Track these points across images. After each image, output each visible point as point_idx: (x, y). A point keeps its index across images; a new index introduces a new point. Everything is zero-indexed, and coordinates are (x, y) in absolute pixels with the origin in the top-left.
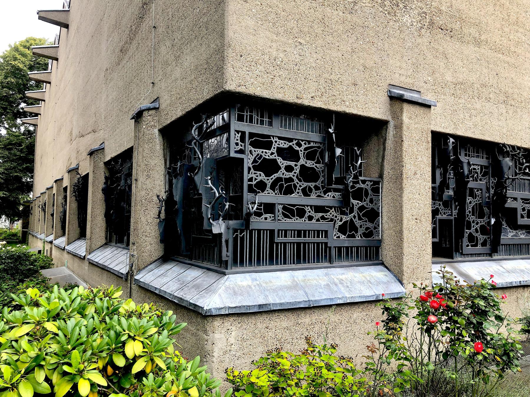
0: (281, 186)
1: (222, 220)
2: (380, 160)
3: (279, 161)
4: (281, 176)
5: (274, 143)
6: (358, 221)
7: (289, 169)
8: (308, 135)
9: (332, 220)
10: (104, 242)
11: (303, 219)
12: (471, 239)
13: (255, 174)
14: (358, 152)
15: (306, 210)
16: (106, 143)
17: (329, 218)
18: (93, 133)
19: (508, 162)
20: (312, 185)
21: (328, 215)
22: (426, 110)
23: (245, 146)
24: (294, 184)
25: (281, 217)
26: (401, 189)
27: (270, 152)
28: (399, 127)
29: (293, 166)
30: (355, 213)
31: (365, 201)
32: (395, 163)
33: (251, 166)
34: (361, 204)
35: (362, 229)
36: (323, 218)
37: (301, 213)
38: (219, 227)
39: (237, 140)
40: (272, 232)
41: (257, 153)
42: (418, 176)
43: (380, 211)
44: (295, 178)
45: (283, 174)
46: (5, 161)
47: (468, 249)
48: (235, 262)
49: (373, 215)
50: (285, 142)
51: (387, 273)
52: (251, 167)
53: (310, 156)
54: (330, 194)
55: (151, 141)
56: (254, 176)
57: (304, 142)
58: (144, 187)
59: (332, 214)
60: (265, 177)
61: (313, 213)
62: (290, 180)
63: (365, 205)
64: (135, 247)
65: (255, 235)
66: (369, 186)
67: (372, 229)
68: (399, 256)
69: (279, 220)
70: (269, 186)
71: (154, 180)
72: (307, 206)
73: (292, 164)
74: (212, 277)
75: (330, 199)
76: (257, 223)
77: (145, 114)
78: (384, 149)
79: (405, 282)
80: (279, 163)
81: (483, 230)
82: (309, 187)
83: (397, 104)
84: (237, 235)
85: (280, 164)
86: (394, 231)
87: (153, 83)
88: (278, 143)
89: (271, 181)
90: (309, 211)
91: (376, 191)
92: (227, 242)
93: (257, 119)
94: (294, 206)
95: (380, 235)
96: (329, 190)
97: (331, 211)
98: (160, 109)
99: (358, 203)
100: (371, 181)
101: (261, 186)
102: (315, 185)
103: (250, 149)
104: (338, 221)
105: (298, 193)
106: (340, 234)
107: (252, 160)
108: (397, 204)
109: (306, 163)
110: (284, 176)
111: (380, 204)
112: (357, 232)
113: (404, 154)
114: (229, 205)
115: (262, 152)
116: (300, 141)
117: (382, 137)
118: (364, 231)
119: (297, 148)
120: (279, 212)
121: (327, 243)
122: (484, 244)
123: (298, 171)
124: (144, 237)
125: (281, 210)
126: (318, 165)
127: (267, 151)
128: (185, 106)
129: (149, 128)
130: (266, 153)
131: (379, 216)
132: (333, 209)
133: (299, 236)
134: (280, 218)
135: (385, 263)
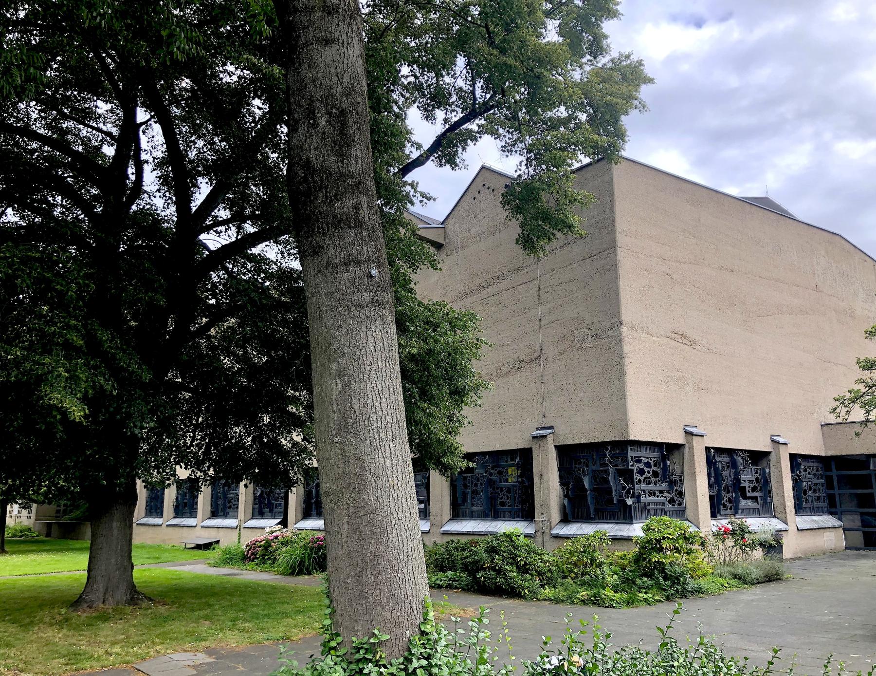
12: (725, 506)
19: (740, 460)
21: (664, 495)
26: (695, 480)
28: (691, 448)
37: (654, 494)
46: (599, 160)
47: (723, 512)
49: (681, 494)
53: (655, 465)
59: (665, 494)
75: (665, 486)
81: (730, 501)
83: (689, 437)
90: (657, 493)
91: (681, 480)
122: (731, 509)
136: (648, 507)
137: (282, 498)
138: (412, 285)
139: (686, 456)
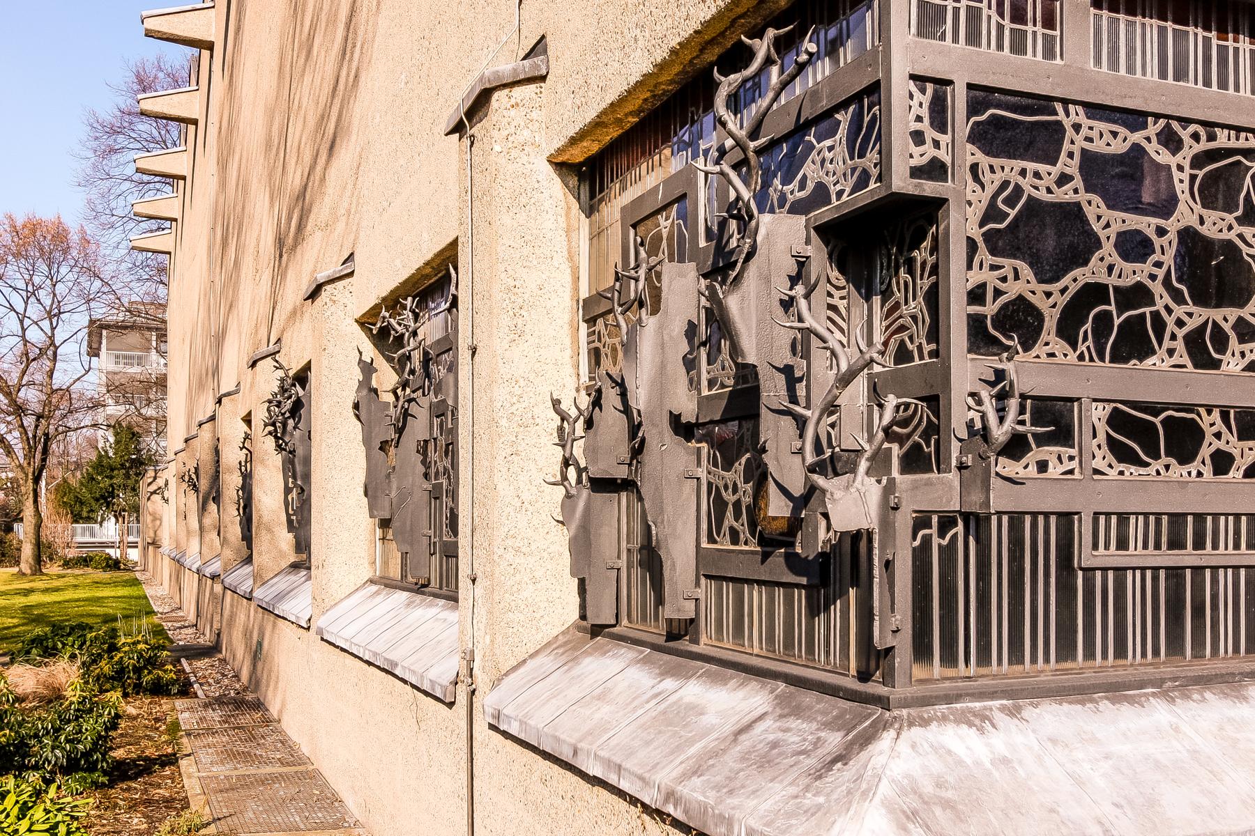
0: (1104, 322)
3: (1091, 213)
4: (1103, 278)
5: (1070, 132)
7: (1134, 247)
11: (1193, 467)
13: (994, 268)
20: (1225, 317)
24: (1156, 316)
27: (1056, 170)
29: (1151, 233)
37: (1183, 439)
39: (919, 119)
41: (999, 177)
44: (1157, 288)
45: (1110, 268)
50: (1115, 128)
55: (523, 200)
60: (1034, 285)
62: (1139, 294)
69: (1096, 472)
70: (1050, 323)
77: (499, 99)
84: (927, 541)
85: (1096, 227)
88: (1084, 131)
89: (1062, 301)
94: (1154, 409)
103: (970, 160)
105: (1171, 352)
109: (1202, 222)
110: (1112, 281)
115: (1023, 173)
123: (1169, 259)
124: (509, 556)
125: (1102, 429)
127: (1042, 168)
129: (514, 153)
130: (1037, 175)
133: (1176, 543)
134: (1098, 463)
136: (1086, 556)
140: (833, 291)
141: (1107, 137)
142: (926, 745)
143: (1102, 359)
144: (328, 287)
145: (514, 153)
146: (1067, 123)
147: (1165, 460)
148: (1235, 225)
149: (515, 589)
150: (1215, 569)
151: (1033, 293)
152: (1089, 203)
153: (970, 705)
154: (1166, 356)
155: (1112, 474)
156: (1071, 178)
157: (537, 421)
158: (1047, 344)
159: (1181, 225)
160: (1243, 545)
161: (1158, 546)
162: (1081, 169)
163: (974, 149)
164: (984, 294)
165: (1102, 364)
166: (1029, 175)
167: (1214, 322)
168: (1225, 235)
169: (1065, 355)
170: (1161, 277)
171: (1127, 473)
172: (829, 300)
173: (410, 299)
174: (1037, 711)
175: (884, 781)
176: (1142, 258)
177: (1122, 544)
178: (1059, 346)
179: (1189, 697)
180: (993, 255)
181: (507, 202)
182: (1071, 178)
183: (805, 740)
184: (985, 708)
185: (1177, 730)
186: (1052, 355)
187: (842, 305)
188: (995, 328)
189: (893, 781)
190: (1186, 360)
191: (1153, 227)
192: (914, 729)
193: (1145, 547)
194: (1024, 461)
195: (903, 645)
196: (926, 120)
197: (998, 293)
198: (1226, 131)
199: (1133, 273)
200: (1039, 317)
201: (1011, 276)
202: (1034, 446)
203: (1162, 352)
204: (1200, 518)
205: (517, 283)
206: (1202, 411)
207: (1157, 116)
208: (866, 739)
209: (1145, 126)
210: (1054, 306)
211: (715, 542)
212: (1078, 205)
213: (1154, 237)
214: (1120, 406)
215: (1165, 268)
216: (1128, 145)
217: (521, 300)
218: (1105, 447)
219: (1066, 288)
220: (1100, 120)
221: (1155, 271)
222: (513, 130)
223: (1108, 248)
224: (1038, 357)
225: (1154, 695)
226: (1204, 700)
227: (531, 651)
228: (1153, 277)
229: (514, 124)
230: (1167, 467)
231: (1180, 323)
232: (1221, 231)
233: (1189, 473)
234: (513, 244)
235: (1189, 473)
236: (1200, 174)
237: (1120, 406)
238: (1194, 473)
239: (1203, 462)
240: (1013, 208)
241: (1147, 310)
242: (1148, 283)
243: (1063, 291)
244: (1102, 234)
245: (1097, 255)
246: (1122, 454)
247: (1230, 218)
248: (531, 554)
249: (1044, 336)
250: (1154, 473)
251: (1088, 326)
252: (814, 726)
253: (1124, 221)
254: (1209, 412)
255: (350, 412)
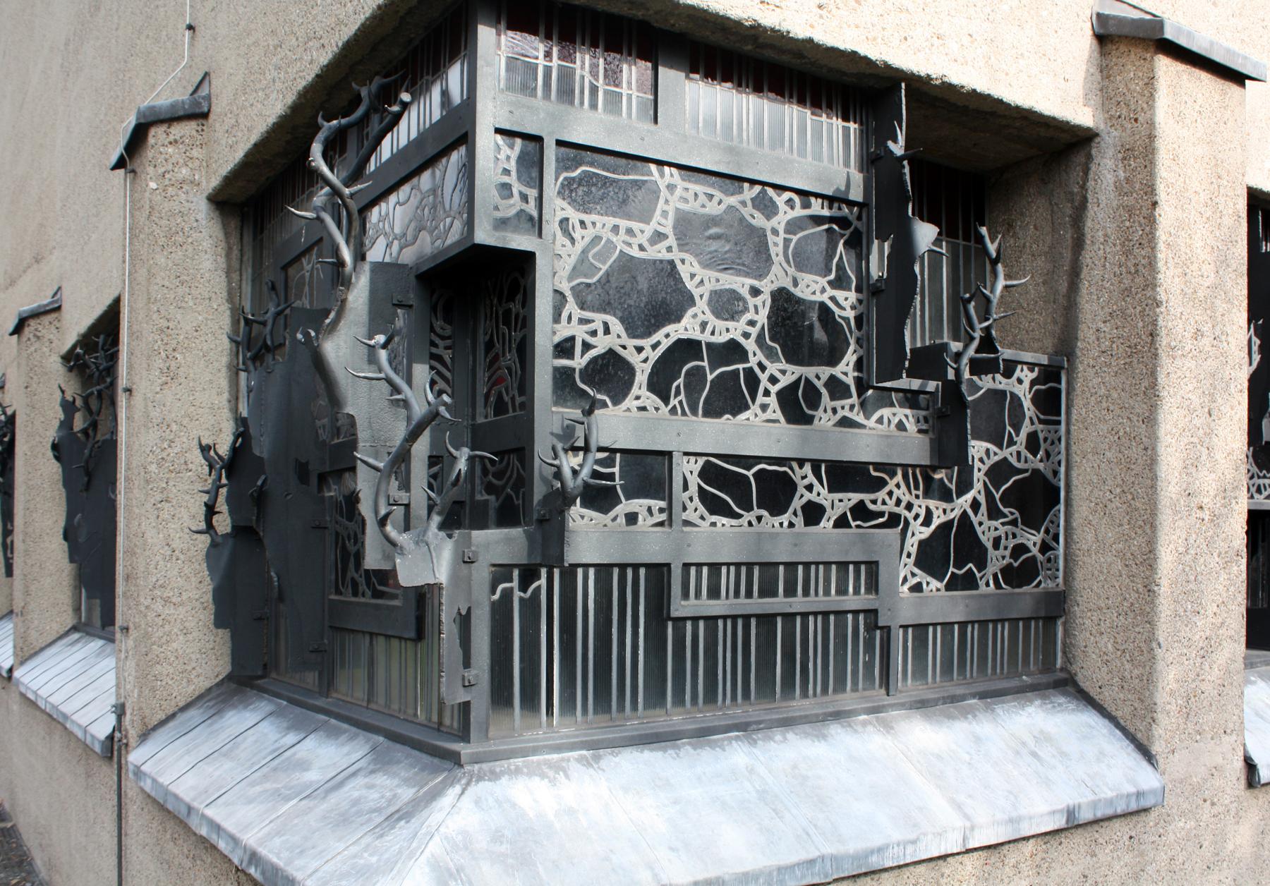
0: (696, 378)
1: (442, 527)
2: (1063, 286)
3: (684, 271)
4: (695, 334)
5: (664, 193)
6: (987, 523)
7: (727, 305)
8: (818, 151)
9: (894, 520)
10: (69, 621)
11: (785, 519)
13: (582, 321)
14: (992, 248)
15: (797, 479)
16: (66, 293)
17: (881, 514)
18: (35, 266)
20: (819, 374)
21: (880, 501)
22: (1233, 88)
23: (540, 199)
24: (750, 373)
25: (695, 510)
26: (1151, 394)
27: (649, 229)
28: (1141, 153)
29: (745, 292)
30: (977, 491)
31: (1012, 442)
32: (1127, 292)
33: (565, 287)
34: (998, 454)
35: (1001, 552)
36: (861, 512)
37: (775, 490)
38: (427, 559)
39: (506, 172)
40: (659, 572)
41: (590, 233)
42: (1206, 342)
43: (1062, 484)
44: (750, 345)
45: (704, 325)
48: (500, 696)
49: (1035, 498)
50: (710, 191)
51: (1090, 718)
52: (568, 293)
54: (886, 412)
55: (180, 239)
56: (580, 333)
57: (787, 195)
58: (155, 414)
60: (625, 340)
61: (822, 495)
62: (733, 351)
63: (1013, 460)
64: (131, 643)
65: (587, 586)
66: (1027, 384)
67: (1035, 551)
68: (1142, 653)
69: (687, 523)
70: (641, 378)
71: (193, 390)
72: (801, 462)
73: (742, 284)
74: (392, 786)
76: (590, 536)
77: (157, 135)
78: (1079, 244)
79: (1157, 748)
80: (685, 277)
82: (808, 381)
84: (508, 594)
85: (690, 285)
86: (1121, 555)
87: (190, 27)
88: (679, 192)
89: (654, 356)
91: (1049, 402)
92: (465, 622)
93: (594, 90)
94: (747, 461)
95: (1061, 574)
96: (885, 397)
97: (891, 485)
98: (212, 116)
99: (988, 451)
100: (1031, 366)
101: (610, 374)
102: (832, 377)
103: (560, 215)
104: (915, 526)
105: (764, 407)
106: (922, 577)
107: (572, 261)
108: (1135, 452)
109: (796, 284)
110: (705, 338)
111: (1063, 457)
112: (982, 566)
113: (1162, 254)
114: (471, 459)
115: (616, 229)
116: (770, 191)
117: (1070, 197)
118: (1007, 560)
119: (759, 220)
120: (686, 487)
121: (875, 612)
123: (762, 318)
124: (158, 607)
125: (694, 481)
126: (840, 295)
127: (635, 226)
128: (292, 71)
129: (171, 190)
130: (630, 232)
131: (1058, 502)
132: (899, 478)
133: (768, 590)
134: (690, 515)
135: (1080, 679)
136: (680, 607)
137: (388, 706)
138: (1154, 645)
139: (1102, 218)
140: (437, 341)
141: (702, 198)
142: (491, 800)
143: (694, 412)
144: (32, 322)
145: (171, 190)
146: (662, 184)
147: (757, 511)
148: (828, 288)
149: (164, 640)
150: (805, 615)
151: (624, 347)
152: (683, 261)
153: (547, 757)
154: (759, 411)
155: (705, 524)
156: (665, 236)
157: (190, 466)
158: (638, 398)
159: (775, 287)
160: (833, 591)
161: (749, 594)
162: (675, 228)
163: (565, 204)
164: (573, 347)
165: (694, 418)
166: (622, 231)
167: (807, 380)
168: (818, 298)
169: (657, 409)
170: (754, 336)
171: (719, 525)
172: (434, 350)
173: (102, 337)
174: (617, 759)
175: (436, 838)
176: (733, 316)
177: (714, 593)
178: (651, 400)
179: (771, 739)
180: (582, 308)
181: (162, 241)
182: (665, 236)
183: (382, 797)
184: (563, 760)
185: (751, 771)
186: (643, 409)
187: (447, 355)
188: (583, 382)
189: (446, 838)
190: (779, 415)
191: (747, 288)
192: (481, 784)
193: (737, 594)
194: (612, 514)
195: (480, 698)
196: (514, 173)
197: (587, 347)
198: (820, 201)
199: (725, 331)
200: (630, 370)
201: (601, 332)
202: (623, 498)
203: (755, 408)
204: (791, 566)
205: (171, 325)
206: (795, 465)
207: (753, 182)
208: (434, 795)
209: (741, 191)
210: (645, 361)
211: (341, 594)
212: (672, 263)
213: (748, 297)
214: (712, 459)
215: (759, 326)
216: (723, 207)
217: (175, 342)
218: (696, 499)
219: (658, 344)
220: (696, 182)
221: (749, 329)
222: (170, 167)
223: (702, 305)
224: (628, 410)
225: (737, 738)
226: (785, 739)
227: (181, 704)
228: (746, 335)
229: (173, 160)
230: (759, 519)
231: (773, 380)
232: (814, 293)
233: (781, 524)
234: (167, 284)
235: (781, 524)
236: (795, 238)
237: (712, 459)
238: (786, 524)
239: (795, 514)
240: (604, 263)
241: (741, 366)
242: (742, 340)
243: (654, 347)
244: (696, 293)
245: (690, 312)
246: (714, 506)
247: (823, 281)
248: (182, 604)
249: (635, 391)
250: (746, 524)
251: (681, 381)
252: (396, 782)
253: (718, 280)
254: (801, 467)
255: (50, 454)
